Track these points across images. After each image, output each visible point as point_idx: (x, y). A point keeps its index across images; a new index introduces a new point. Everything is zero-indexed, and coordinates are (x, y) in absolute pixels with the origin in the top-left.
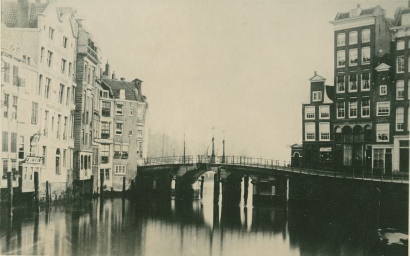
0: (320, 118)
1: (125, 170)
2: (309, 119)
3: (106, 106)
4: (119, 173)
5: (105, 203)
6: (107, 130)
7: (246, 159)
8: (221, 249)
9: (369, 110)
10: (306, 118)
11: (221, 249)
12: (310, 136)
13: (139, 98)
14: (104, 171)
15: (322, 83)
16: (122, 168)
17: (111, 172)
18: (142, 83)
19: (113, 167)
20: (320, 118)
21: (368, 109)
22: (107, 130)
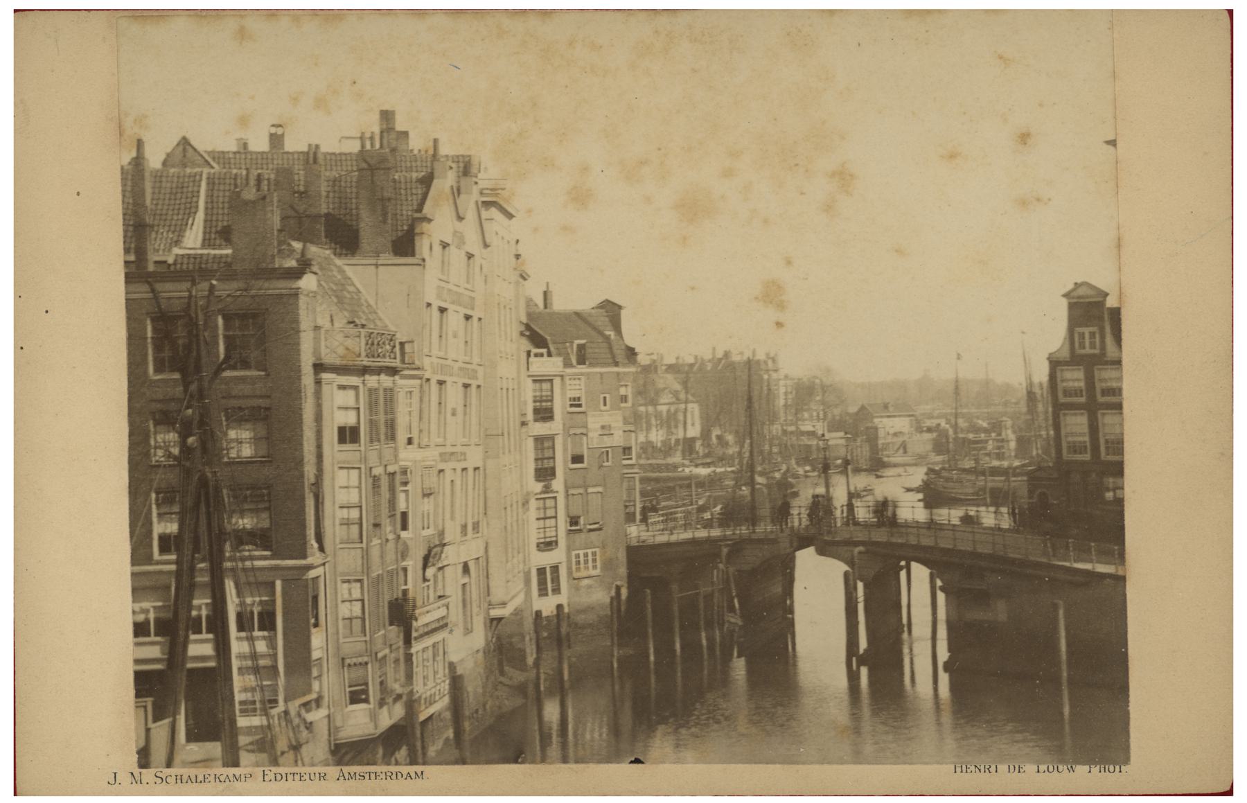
0: (1101, 399)
1: (598, 564)
2: (1069, 400)
3: (541, 390)
4: (583, 573)
5: (276, 742)
6: (549, 458)
7: (504, 380)
8: (957, 370)
9: (1088, 444)
10: (1062, 399)
11: (957, 370)
12: (1075, 449)
13: (620, 354)
14: (545, 573)
15: (1101, 304)
16: (590, 558)
17: (563, 572)
18: (623, 312)
19: (569, 561)
20: (1101, 399)
21: (1085, 442)
22: (549, 458)
